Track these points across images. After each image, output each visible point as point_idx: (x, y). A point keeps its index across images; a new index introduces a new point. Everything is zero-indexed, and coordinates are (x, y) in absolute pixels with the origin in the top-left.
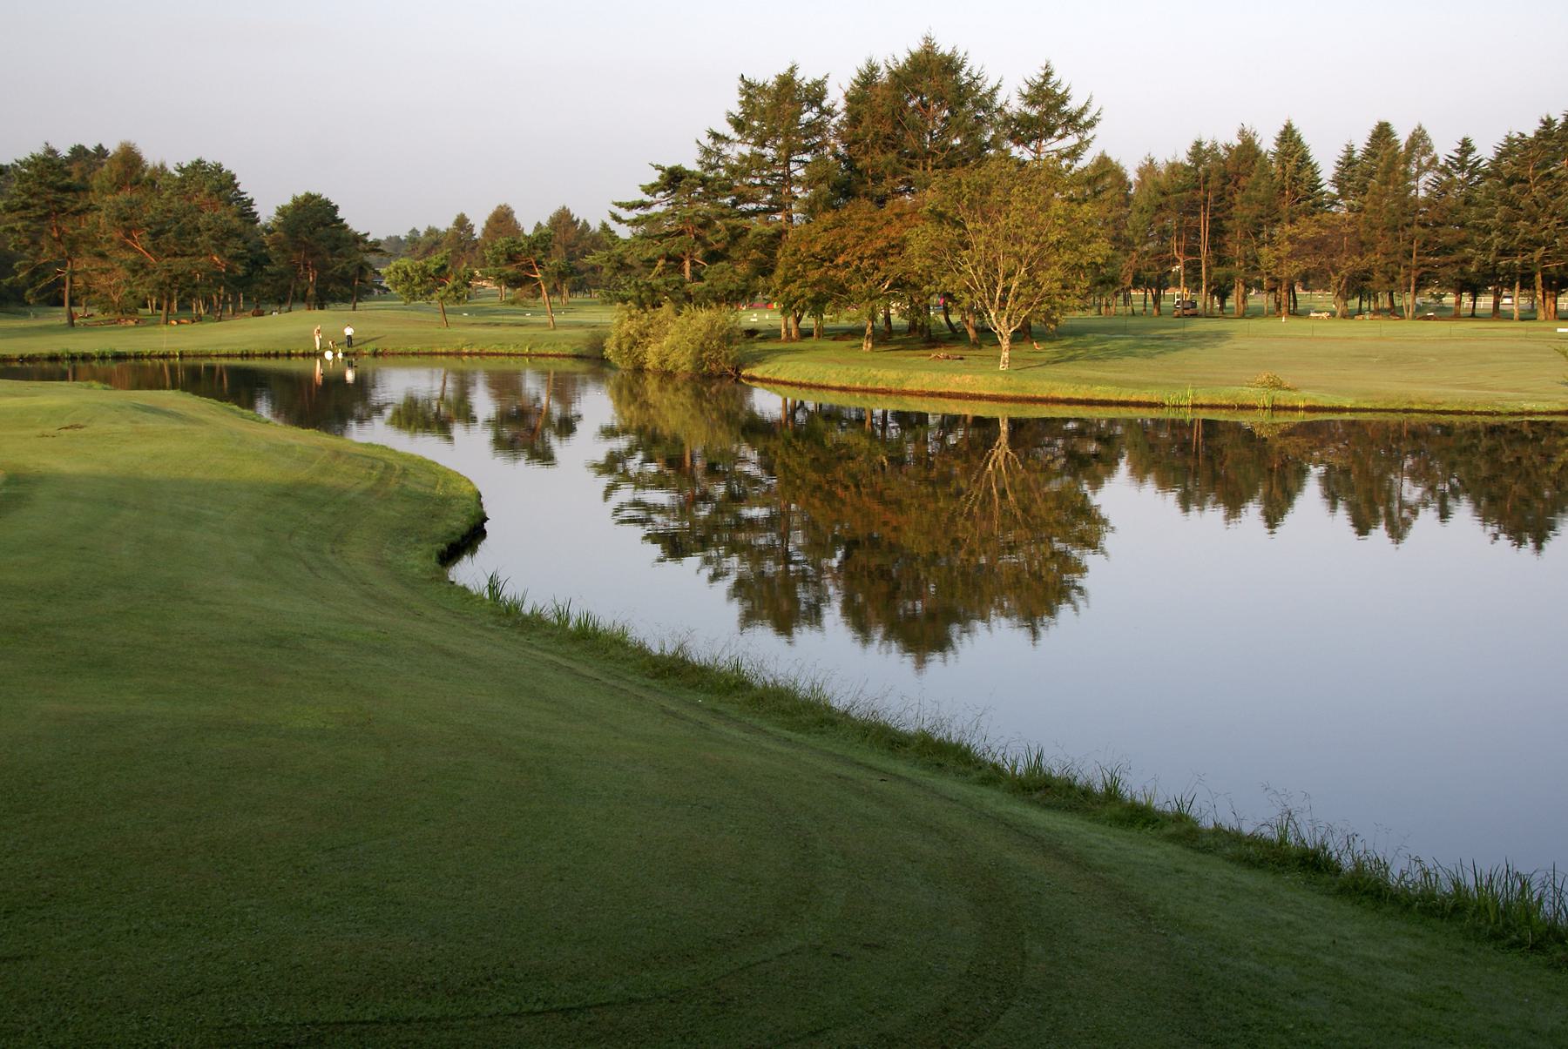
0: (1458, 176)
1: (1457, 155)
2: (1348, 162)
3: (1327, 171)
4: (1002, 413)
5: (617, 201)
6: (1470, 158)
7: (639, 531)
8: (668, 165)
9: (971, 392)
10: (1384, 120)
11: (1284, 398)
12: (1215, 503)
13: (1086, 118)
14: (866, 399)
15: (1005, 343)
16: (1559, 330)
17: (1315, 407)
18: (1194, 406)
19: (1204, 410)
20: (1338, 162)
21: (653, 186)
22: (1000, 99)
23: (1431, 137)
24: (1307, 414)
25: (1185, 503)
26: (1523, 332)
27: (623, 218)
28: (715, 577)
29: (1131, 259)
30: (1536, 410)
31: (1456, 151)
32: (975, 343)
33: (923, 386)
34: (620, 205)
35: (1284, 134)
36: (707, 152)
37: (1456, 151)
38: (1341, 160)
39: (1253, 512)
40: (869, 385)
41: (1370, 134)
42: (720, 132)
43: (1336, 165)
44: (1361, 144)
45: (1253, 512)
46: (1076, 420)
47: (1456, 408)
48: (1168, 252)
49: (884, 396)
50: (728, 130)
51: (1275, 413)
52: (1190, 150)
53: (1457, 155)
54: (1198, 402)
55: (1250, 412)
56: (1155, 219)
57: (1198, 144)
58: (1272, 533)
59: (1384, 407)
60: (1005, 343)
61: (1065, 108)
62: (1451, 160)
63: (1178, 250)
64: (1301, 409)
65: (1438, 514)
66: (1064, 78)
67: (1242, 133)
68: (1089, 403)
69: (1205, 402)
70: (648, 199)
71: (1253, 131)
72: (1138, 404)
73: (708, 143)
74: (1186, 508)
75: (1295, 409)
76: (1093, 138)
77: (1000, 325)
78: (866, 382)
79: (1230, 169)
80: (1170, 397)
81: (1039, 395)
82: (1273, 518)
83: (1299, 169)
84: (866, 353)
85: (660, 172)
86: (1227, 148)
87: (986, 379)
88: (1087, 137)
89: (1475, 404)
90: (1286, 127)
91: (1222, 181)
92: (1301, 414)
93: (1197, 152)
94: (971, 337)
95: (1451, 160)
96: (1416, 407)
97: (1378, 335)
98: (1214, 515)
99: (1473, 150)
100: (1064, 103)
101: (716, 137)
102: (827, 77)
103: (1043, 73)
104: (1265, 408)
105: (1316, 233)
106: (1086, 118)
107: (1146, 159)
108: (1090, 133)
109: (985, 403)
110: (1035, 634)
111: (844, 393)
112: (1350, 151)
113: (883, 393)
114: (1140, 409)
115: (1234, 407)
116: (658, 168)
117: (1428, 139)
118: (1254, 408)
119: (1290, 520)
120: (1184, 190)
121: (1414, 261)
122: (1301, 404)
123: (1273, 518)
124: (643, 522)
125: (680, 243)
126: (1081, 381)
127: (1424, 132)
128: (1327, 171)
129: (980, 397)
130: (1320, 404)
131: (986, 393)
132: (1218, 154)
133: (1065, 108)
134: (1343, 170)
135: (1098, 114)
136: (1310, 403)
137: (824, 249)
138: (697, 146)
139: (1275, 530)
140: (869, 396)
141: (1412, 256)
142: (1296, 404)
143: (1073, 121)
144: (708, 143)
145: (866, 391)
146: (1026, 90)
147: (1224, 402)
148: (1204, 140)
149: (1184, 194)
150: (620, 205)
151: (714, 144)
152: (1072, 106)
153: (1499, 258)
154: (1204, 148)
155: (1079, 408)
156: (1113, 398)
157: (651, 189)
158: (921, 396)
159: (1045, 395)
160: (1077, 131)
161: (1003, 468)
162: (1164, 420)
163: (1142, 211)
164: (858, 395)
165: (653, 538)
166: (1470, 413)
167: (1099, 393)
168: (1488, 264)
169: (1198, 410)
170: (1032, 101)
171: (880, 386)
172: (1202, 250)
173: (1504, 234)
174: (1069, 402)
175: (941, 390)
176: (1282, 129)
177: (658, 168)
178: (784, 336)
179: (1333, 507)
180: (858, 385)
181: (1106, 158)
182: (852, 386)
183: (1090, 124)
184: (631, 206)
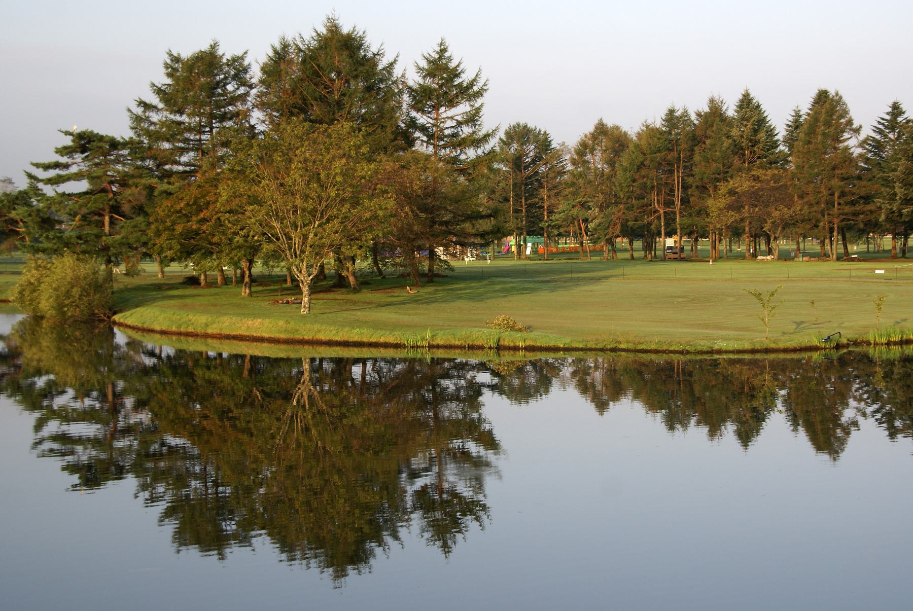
0: (891, 136)
1: (888, 117)
2: (796, 125)
3: (781, 132)
4: (306, 353)
5: (35, 162)
6: (899, 119)
7: (57, 463)
8: (76, 129)
9: (255, 335)
10: (823, 87)
11: (508, 338)
12: (698, 423)
13: (475, 88)
14: (180, 341)
15: (305, 290)
16: (877, 272)
17: (534, 346)
18: (431, 347)
19: (441, 351)
20: (787, 125)
21: (65, 148)
22: (397, 72)
23: (847, 102)
24: (528, 354)
25: (672, 422)
26: (847, 273)
27: (40, 177)
28: (153, 499)
29: (619, 212)
30: (724, 348)
31: (888, 114)
32: (354, 288)
33: (221, 329)
34: (37, 165)
35: (742, 101)
36: (138, 119)
37: (888, 114)
38: (790, 123)
39: (729, 429)
40: (182, 330)
41: (812, 100)
42: (148, 101)
43: (785, 127)
44: (805, 107)
45: (729, 429)
46: (404, 360)
47: (653, 347)
48: (651, 205)
49: (193, 339)
50: (154, 100)
51: (502, 353)
52: (664, 117)
53: (888, 117)
54: (435, 343)
55: (479, 352)
56: (637, 177)
57: (671, 112)
58: (746, 449)
59: (594, 346)
60: (305, 290)
61: (457, 81)
62: (883, 122)
63: (658, 203)
64: (522, 349)
65: (887, 433)
66: (457, 56)
67: (712, 101)
68: (346, 344)
69: (441, 342)
70: (64, 160)
71: (721, 99)
72: (386, 345)
73: (139, 111)
74: (671, 428)
75: (516, 349)
76: (482, 105)
77: (300, 272)
78: (180, 326)
79: (699, 133)
80: (409, 338)
81: (306, 337)
82: (746, 436)
83: (755, 132)
84: (243, 298)
85: (71, 138)
86: (699, 115)
87: (270, 323)
88: (477, 105)
89: (670, 344)
90: (744, 95)
91: (690, 143)
92: (521, 353)
93: (671, 118)
94: (352, 283)
95: (883, 122)
96: (623, 346)
97: (729, 277)
98: (696, 433)
99: (904, 113)
100: (457, 75)
101: (147, 106)
102: (246, 53)
103: (438, 49)
104: (490, 348)
105: (750, 187)
106: (475, 88)
107: (643, 125)
108: (479, 102)
109: (265, 345)
110: (446, 548)
111: (164, 337)
112: (798, 115)
113: (192, 336)
114: (387, 350)
115: (464, 347)
116: (67, 133)
117: (844, 104)
118: (481, 348)
119: (760, 442)
120: (659, 151)
121: (835, 210)
122: (521, 344)
123: (746, 436)
124: (63, 454)
125: (95, 201)
126: (377, 326)
127: (841, 98)
128: (781, 132)
129: (261, 340)
130: (538, 344)
131: (266, 335)
132: (689, 119)
133: (457, 81)
134: (792, 132)
135: (485, 85)
136: (529, 343)
137: (188, 204)
138: (129, 114)
139: (748, 447)
140: (182, 338)
141: (834, 206)
142: (517, 344)
143: (468, 92)
144: (139, 111)
145: (180, 334)
146: (424, 64)
147: (458, 343)
148: (676, 108)
149: (658, 154)
150: (37, 165)
151: (144, 112)
152: (465, 79)
153: (904, 206)
154: (677, 114)
155: (338, 349)
156: (365, 340)
157: (65, 151)
158: (220, 338)
159: (311, 337)
160: (469, 100)
161: (307, 403)
162: (348, 359)
163: (625, 170)
164: (174, 338)
165: (72, 468)
166: (664, 352)
167: (355, 335)
168: (894, 212)
169: (435, 350)
170: (430, 74)
171: (190, 329)
172: (676, 203)
173: (905, 185)
174: (330, 343)
175: (234, 333)
176: (741, 97)
177: (67, 133)
178: (203, 283)
179: (795, 430)
180: (174, 329)
181: (603, 125)
182: (170, 330)
183: (479, 94)
184: (47, 167)
